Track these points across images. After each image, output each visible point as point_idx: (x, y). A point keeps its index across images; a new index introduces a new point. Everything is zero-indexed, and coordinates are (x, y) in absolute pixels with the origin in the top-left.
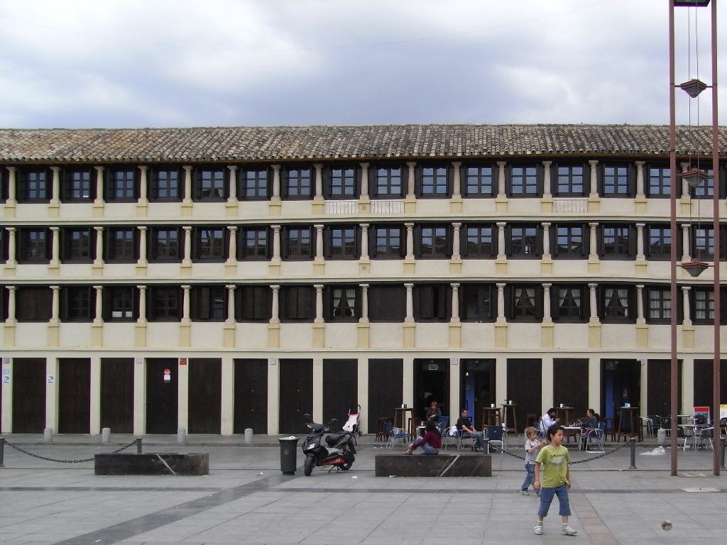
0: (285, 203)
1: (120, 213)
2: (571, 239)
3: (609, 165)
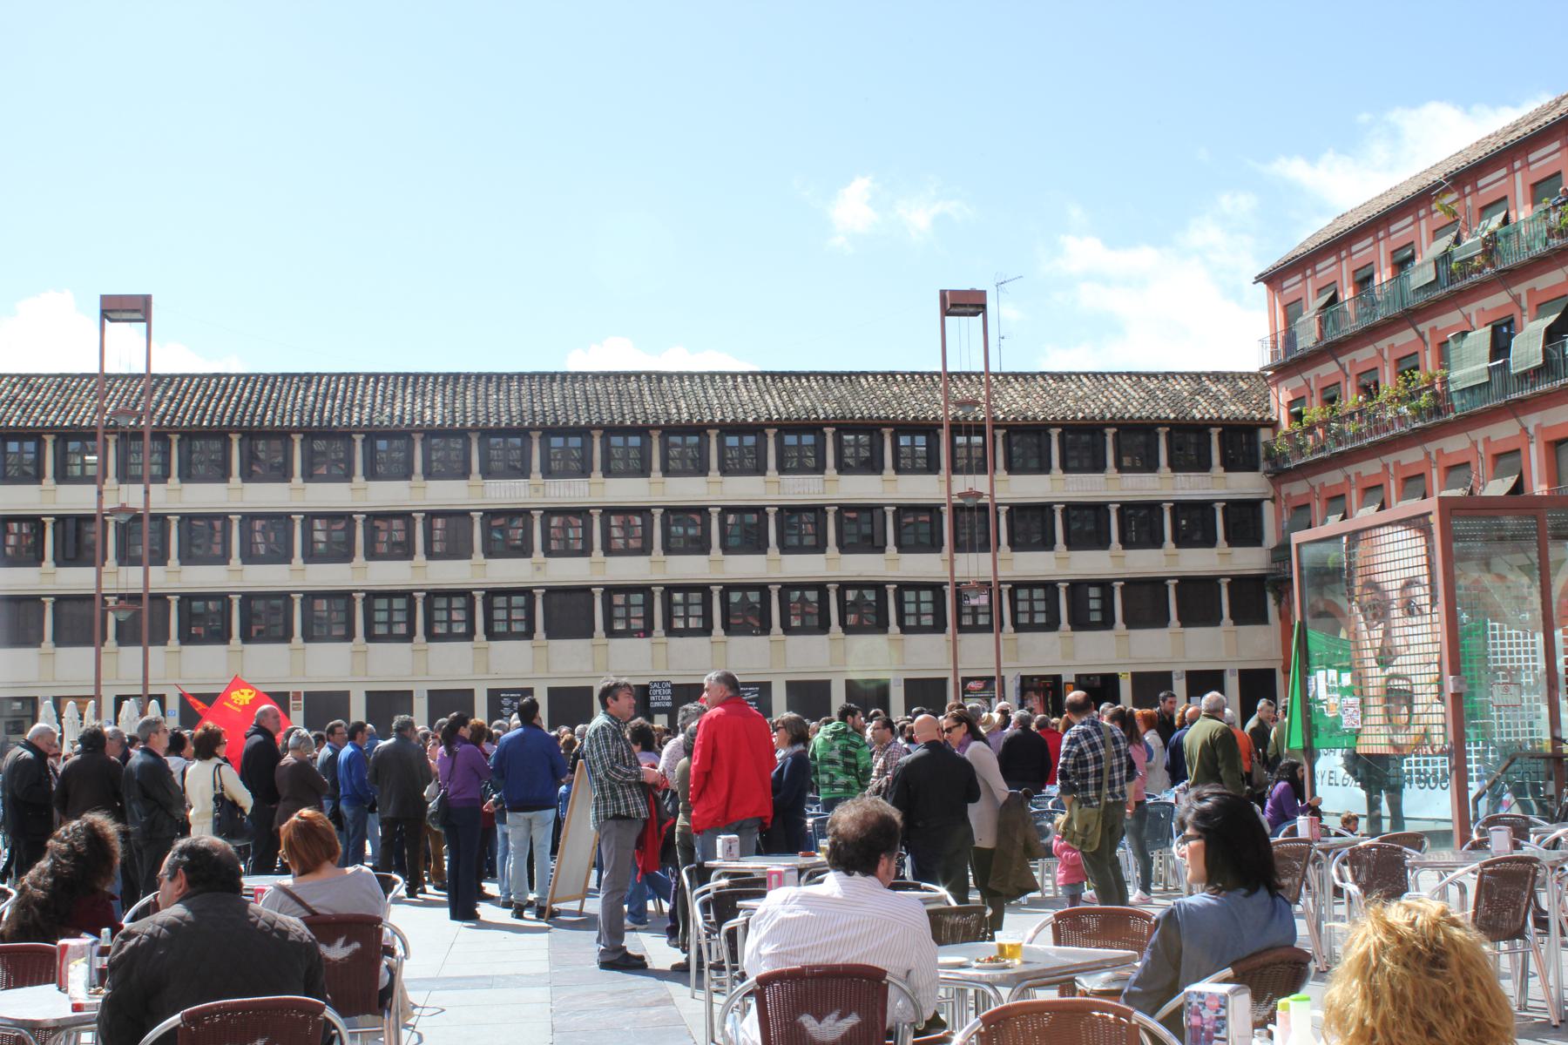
0: (310, 486)
1: (76, 499)
2: (801, 527)
3: (905, 433)
